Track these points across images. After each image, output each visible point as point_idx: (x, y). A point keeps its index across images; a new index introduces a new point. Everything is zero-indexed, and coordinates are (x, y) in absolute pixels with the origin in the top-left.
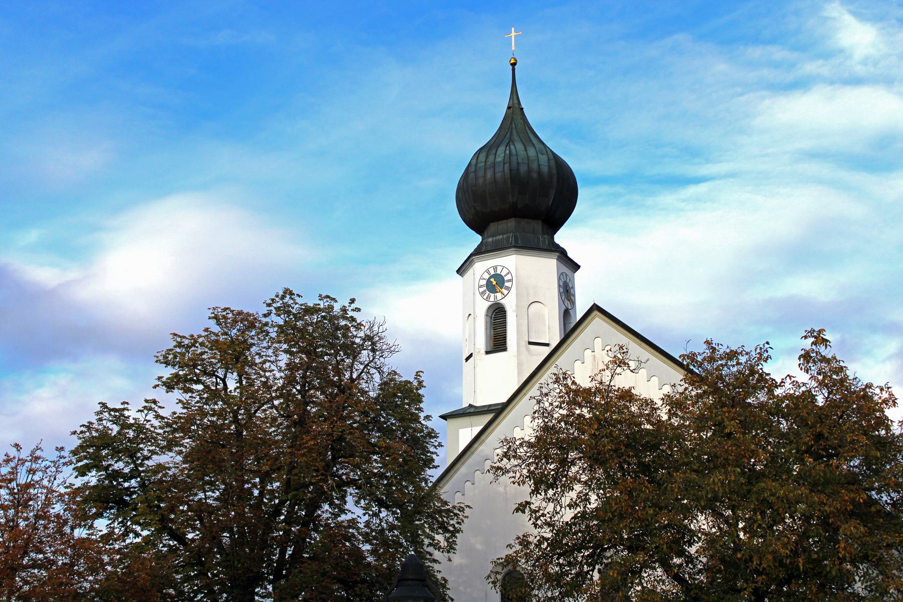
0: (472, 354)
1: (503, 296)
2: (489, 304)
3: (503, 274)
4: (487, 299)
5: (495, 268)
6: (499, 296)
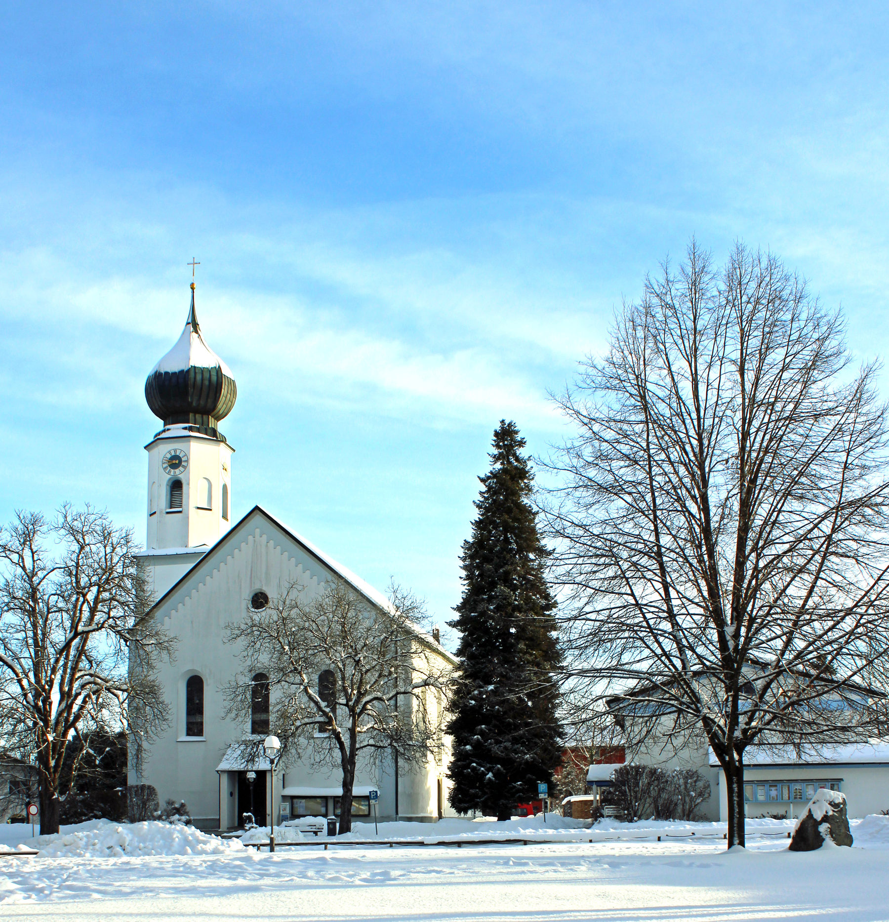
4: (169, 473)
5: (175, 451)
6: (177, 471)
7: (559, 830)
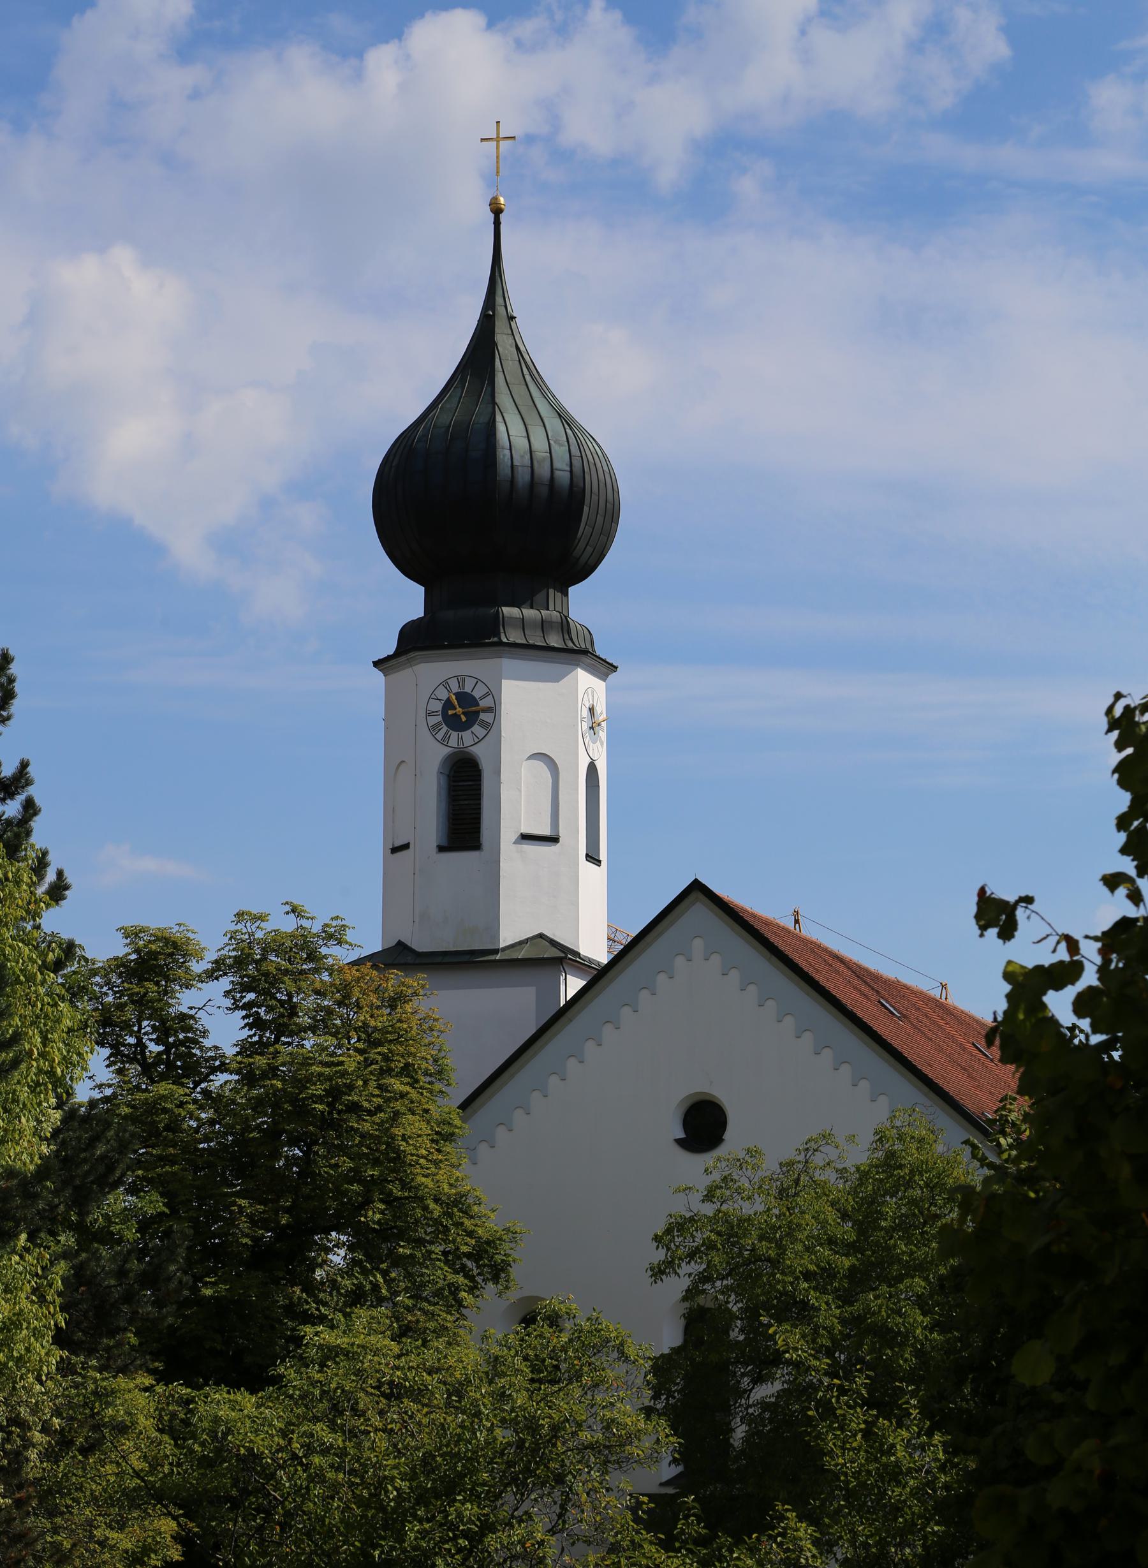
0: (408, 844)
1: (477, 740)
2: (446, 751)
3: (477, 694)
4: (444, 741)
5: (461, 680)
6: (467, 736)
7: (99, 1096)
